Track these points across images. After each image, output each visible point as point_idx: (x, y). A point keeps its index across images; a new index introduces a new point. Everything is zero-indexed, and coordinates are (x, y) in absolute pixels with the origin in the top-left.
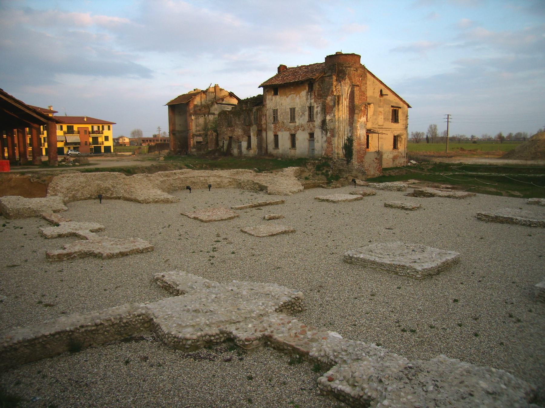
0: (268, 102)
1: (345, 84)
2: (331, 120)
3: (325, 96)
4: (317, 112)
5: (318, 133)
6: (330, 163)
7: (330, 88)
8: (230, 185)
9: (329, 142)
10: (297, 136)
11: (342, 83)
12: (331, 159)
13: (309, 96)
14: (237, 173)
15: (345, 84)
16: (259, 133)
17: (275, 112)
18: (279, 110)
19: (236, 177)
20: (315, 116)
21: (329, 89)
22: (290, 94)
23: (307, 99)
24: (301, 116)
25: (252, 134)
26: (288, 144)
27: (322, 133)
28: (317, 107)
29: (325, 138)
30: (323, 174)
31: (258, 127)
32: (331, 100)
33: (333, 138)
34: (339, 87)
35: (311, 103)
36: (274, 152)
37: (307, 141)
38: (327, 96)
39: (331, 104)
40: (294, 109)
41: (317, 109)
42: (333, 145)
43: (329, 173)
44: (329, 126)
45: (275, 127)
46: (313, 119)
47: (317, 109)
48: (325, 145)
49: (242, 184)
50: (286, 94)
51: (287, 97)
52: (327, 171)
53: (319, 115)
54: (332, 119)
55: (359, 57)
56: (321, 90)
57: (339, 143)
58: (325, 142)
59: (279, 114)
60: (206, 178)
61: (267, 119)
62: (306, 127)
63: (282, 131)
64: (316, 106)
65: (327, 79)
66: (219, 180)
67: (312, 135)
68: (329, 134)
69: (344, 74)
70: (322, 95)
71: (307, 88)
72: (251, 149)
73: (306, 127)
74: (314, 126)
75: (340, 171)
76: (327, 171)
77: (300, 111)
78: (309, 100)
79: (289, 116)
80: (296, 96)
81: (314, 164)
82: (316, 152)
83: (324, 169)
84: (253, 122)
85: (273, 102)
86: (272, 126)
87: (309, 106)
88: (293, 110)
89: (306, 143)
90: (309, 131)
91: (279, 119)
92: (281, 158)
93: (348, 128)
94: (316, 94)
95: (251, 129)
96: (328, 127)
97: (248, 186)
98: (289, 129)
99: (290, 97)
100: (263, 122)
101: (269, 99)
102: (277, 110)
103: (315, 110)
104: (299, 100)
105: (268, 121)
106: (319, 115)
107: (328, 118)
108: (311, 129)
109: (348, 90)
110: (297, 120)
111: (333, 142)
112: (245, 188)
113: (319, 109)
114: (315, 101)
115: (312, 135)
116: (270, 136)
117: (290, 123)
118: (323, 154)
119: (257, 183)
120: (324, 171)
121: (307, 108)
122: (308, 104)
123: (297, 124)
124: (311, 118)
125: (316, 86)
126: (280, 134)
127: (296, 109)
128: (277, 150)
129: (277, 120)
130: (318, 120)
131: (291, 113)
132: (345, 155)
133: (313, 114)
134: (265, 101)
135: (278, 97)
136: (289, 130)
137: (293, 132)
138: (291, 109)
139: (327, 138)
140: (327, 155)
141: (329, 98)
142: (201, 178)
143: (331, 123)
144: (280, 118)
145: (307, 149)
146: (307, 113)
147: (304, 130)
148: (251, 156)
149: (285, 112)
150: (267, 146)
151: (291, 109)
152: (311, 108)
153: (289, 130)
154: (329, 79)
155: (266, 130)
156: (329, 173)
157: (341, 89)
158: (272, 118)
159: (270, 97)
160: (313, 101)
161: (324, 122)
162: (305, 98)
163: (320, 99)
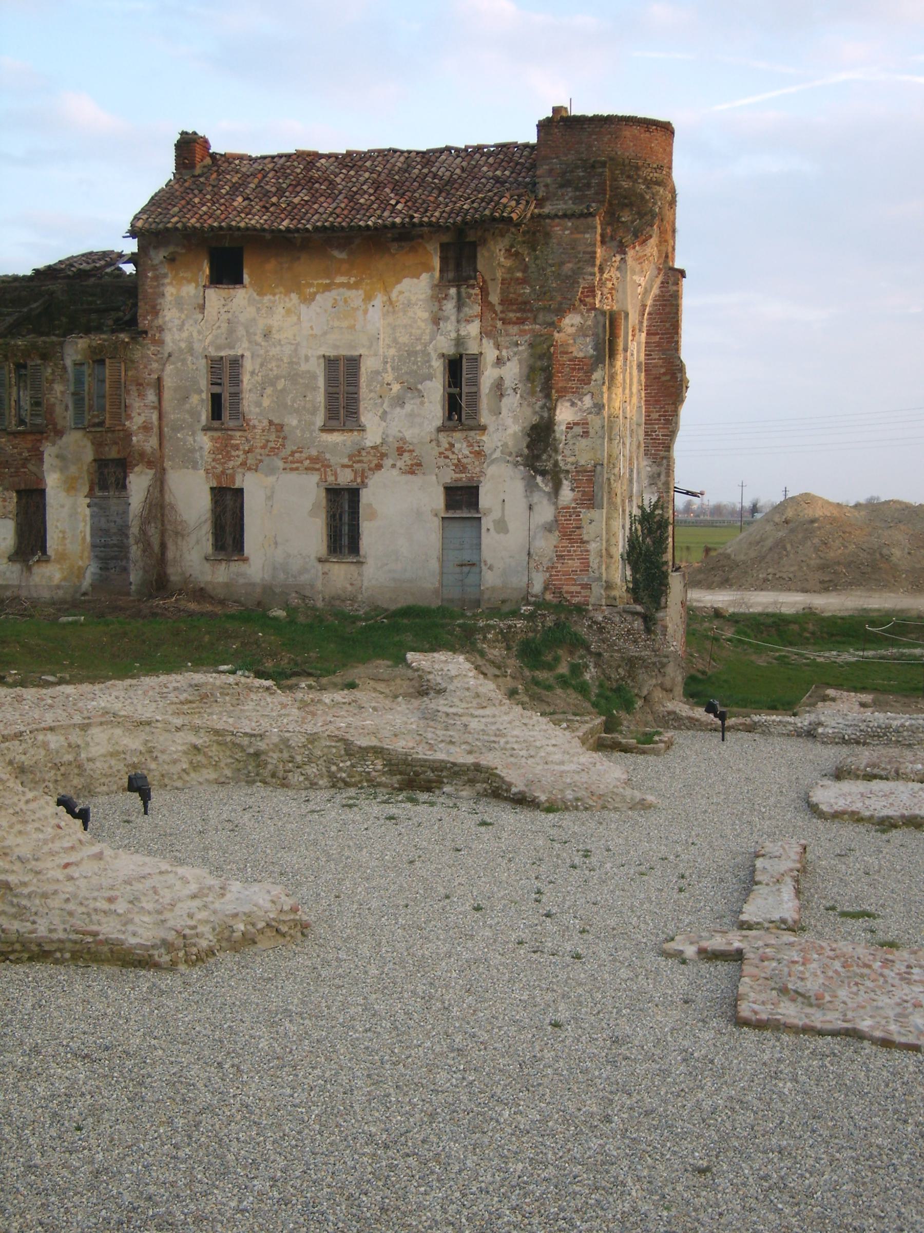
0: (170, 315)
1: (640, 260)
2: (582, 428)
3: (547, 309)
4: (499, 385)
5: (503, 489)
6: (582, 629)
7: (577, 273)
8: (196, 767)
9: (567, 529)
10: (366, 497)
11: (631, 253)
12: (580, 609)
13: (450, 306)
14: (204, 697)
15: (640, 260)
16: (109, 475)
17: (224, 373)
18: (248, 365)
19: (219, 719)
20: (485, 402)
21: (572, 280)
22: (328, 288)
23: (436, 320)
24: (400, 402)
25: (52, 481)
26: (311, 535)
27: (531, 486)
28: (499, 362)
29: (545, 512)
30: (564, 682)
31: (98, 445)
32: (582, 331)
33: (594, 514)
34: (614, 273)
35: (459, 341)
36: (219, 575)
37: (436, 523)
38: (561, 312)
39: (583, 349)
40: (353, 363)
41: (501, 368)
42: (593, 546)
43: (587, 676)
44: (572, 453)
45: (224, 450)
46: (475, 413)
47: (501, 368)
48: (546, 545)
49: (273, 758)
50: (295, 287)
51: (308, 300)
52: (576, 670)
53: (511, 401)
54: (584, 423)
55: (184, 134)
56: (524, 281)
57: (611, 534)
58: (548, 528)
59: (247, 381)
60: (75, 737)
61: (167, 405)
62: (430, 454)
63: (271, 471)
64: (490, 354)
65: (562, 231)
66: (133, 742)
67: (462, 498)
68: (567, 495)
69: (641, 215)
70: (530, 306)
71: (436, 263)
72: (45, 559)
73: (430, 454)
74: (479, 454)
75: (631, 663)
76: (576, 670)
77: (389, 377)
78: (449, 326)
79: (320, 398)
80: (368, 298)
81: (506, 637)
82: (490, 579)
83: (557, 659)
84: (65, 415)
85: (192, 318)
86: (205, 441)
87: (450, 350)
88: (343, 375)
89: (430, 535)
90: (449, 476)
91: (249, 403)
92: (286, 606)
93: (644, 466)
94: (494, 298)
95: (49, 452)
96: (565, 460)
97: (311, 770)
98: (314, 460)
99: (324, 300)
100: (140, 414)
101: (179, 303)
102: (236, 363)
103: (488, 375)
104: (394, 319)
105: (173, 415)
106: (511, 401)
107: (565, 414)
108: (460, 467)
109: (646, 292)
110: (368, 418)
111: (588, 532)
112: (295, 778)
113: (512, 371)
114: (485, 333)
115: (462, 498)
116: (191, 496)
117: (325, 429)
118: (537, 588)
119: (378, 751)
120: (563, 669)
121: (438, 365)
122: (444, 344)
123: (372, 437)
124: (459, 409)
125: (495, 259)
126: (255, 488)
127: (368, 366)
128: (235, 567)
129: (237, 413)
130: (505, 422)
131: (331, 381)
132: (635, 592)
133: (475, 396)
134: (155, 311)
135: (241, 297)
136: (318, 464)
137: (345, 478)
138: (331, 363)
139: (559, 510)
140: (558, 592)
141: (571, 322)
142: (55, 741)
143: (584, 442)
144: (255, 403)
145: (434, 565)
146: (435, 389)
147: (414, 469)
148: (46, 595)
149: (293, 377)
150: (163, 546)
151: (331, 363)
152: (457, 368)
153: (318, 464)
154: (576, 229)
155: (156, 463)
156: (587, 676)
157: (623, 279)
158: (200, 402)
159: (189, 290)
160: (473, 329)
161: (540, 437)
162: (422, 314)
163: (521, 321)
